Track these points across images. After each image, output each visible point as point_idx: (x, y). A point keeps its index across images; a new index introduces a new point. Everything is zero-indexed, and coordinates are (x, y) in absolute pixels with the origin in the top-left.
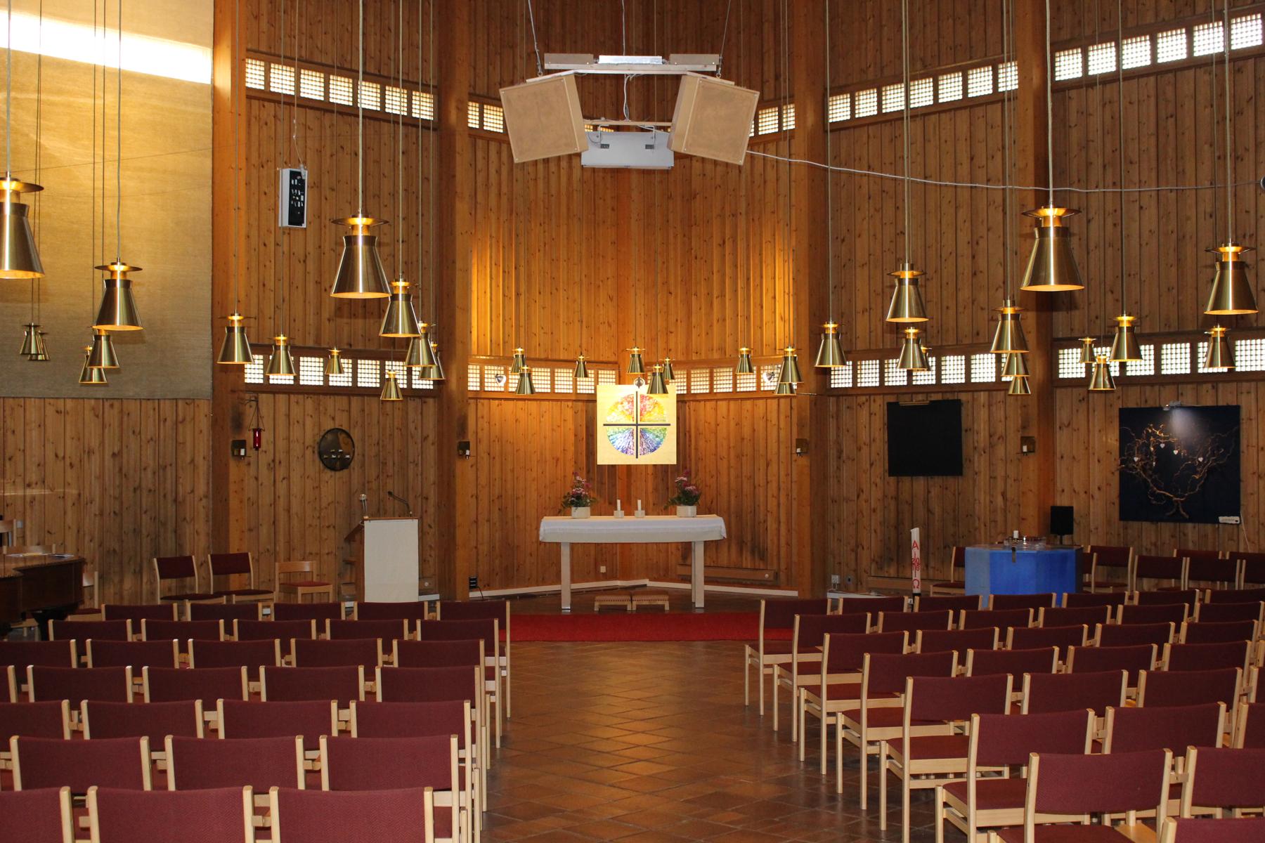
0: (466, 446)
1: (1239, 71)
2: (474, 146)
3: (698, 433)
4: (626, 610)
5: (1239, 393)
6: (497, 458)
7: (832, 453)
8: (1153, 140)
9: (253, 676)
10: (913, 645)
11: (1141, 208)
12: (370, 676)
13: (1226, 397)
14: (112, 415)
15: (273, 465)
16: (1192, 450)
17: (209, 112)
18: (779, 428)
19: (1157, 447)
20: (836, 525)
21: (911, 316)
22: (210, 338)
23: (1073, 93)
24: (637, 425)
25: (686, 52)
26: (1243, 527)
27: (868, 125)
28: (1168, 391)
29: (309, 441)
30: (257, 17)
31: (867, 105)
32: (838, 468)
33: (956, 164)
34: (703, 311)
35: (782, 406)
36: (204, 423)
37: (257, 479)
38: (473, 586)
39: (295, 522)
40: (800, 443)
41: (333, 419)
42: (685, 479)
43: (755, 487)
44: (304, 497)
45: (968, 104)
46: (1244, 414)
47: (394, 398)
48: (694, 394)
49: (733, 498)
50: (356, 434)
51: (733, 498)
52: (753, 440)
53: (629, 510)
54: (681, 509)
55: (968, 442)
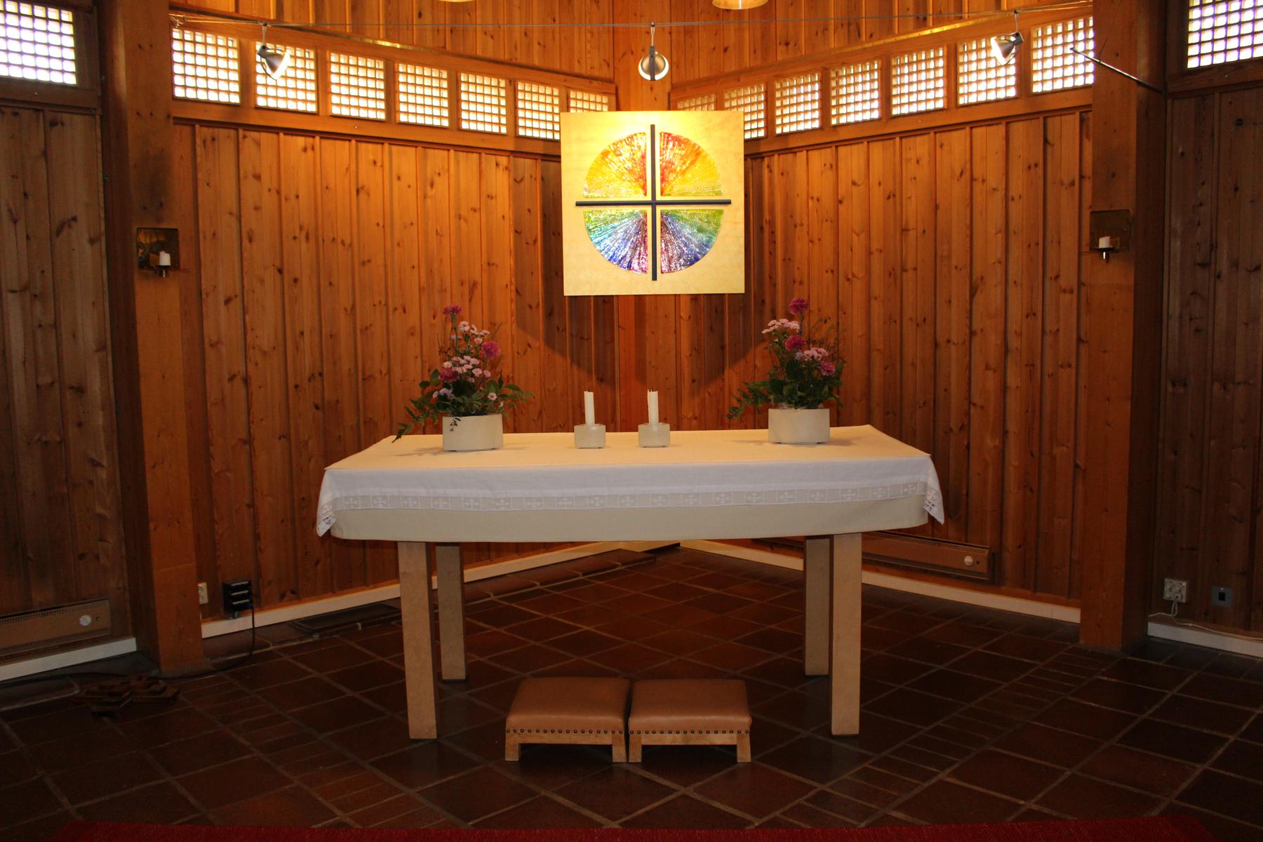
4: (609, 762)
6: (305, 281)
18: (1007, 198)
24: (654, 204)
42: (794, 325)
43: (936, 345)
48: (783, 135)
49: (877, 370)
51: (877, 370)
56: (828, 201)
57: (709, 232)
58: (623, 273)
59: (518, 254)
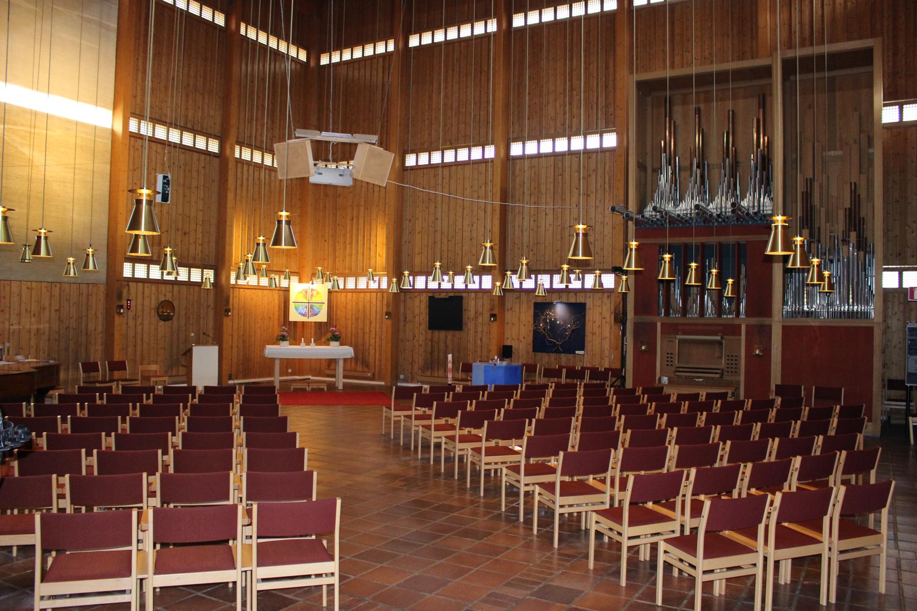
0: (228, 311)
1: (590, 158)
2: (237, 166)
3: (337, 307)
5: (586, 297)
7: (402, 318)
8: (552, 185)
9: (64, 421)
11: (546, 214)
12: (124, 421)
13: (581, 299)
14: (56, 291)
15: (135, 318)
16: (565, 322)
17: (110, 142)
19: (550, 320)
20: (403, 352)
21: (489, 263)
22: (106, 254)
23: (518, 161)
25: (363, 133)
26: (586, 355)
27: (424, 168)
28: (555, 296)
29: (153, 306)
30: (135, 97)
31: (424, 159)
32: (404, 326)
33: (464, 189)
34: (342, 250)
35: (378, 296)
36: (102, 296)
37: (127, 324)
38: (230, 379)
39: (145, 346)
40: (387, 314)
41: (165, 295)
44: (150, 334)
45: (469, 163)
46: (587, 306)
47: (208, 287)
49: (353, 338)
50: (176, 304)
51: (353, 338)
52: (364, 311)
53: (308, 343)
54: (332, 343)
55: (465, 315)
56: (345, 303)
57: (320, 309)
58: (302, 317)
59: (279, 311)
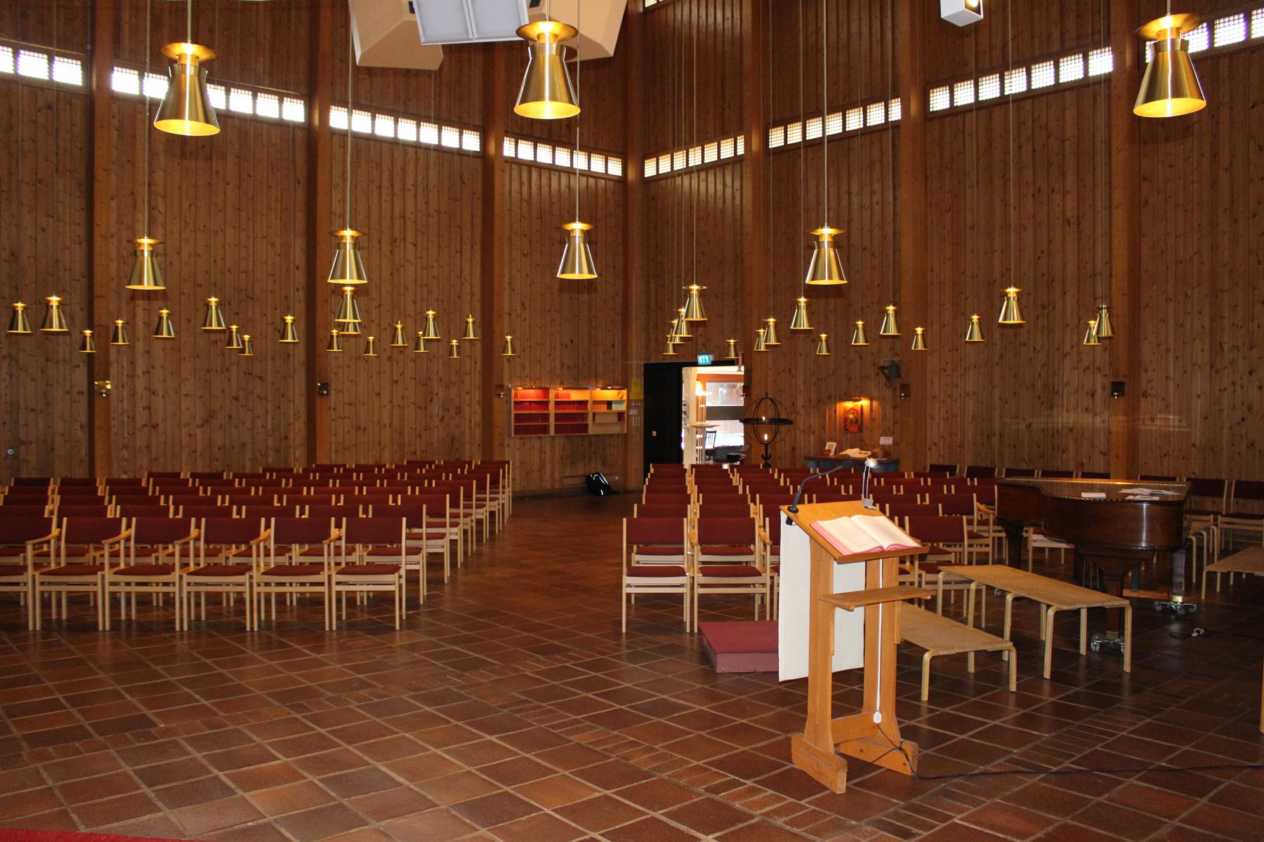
10: (268, 530)
